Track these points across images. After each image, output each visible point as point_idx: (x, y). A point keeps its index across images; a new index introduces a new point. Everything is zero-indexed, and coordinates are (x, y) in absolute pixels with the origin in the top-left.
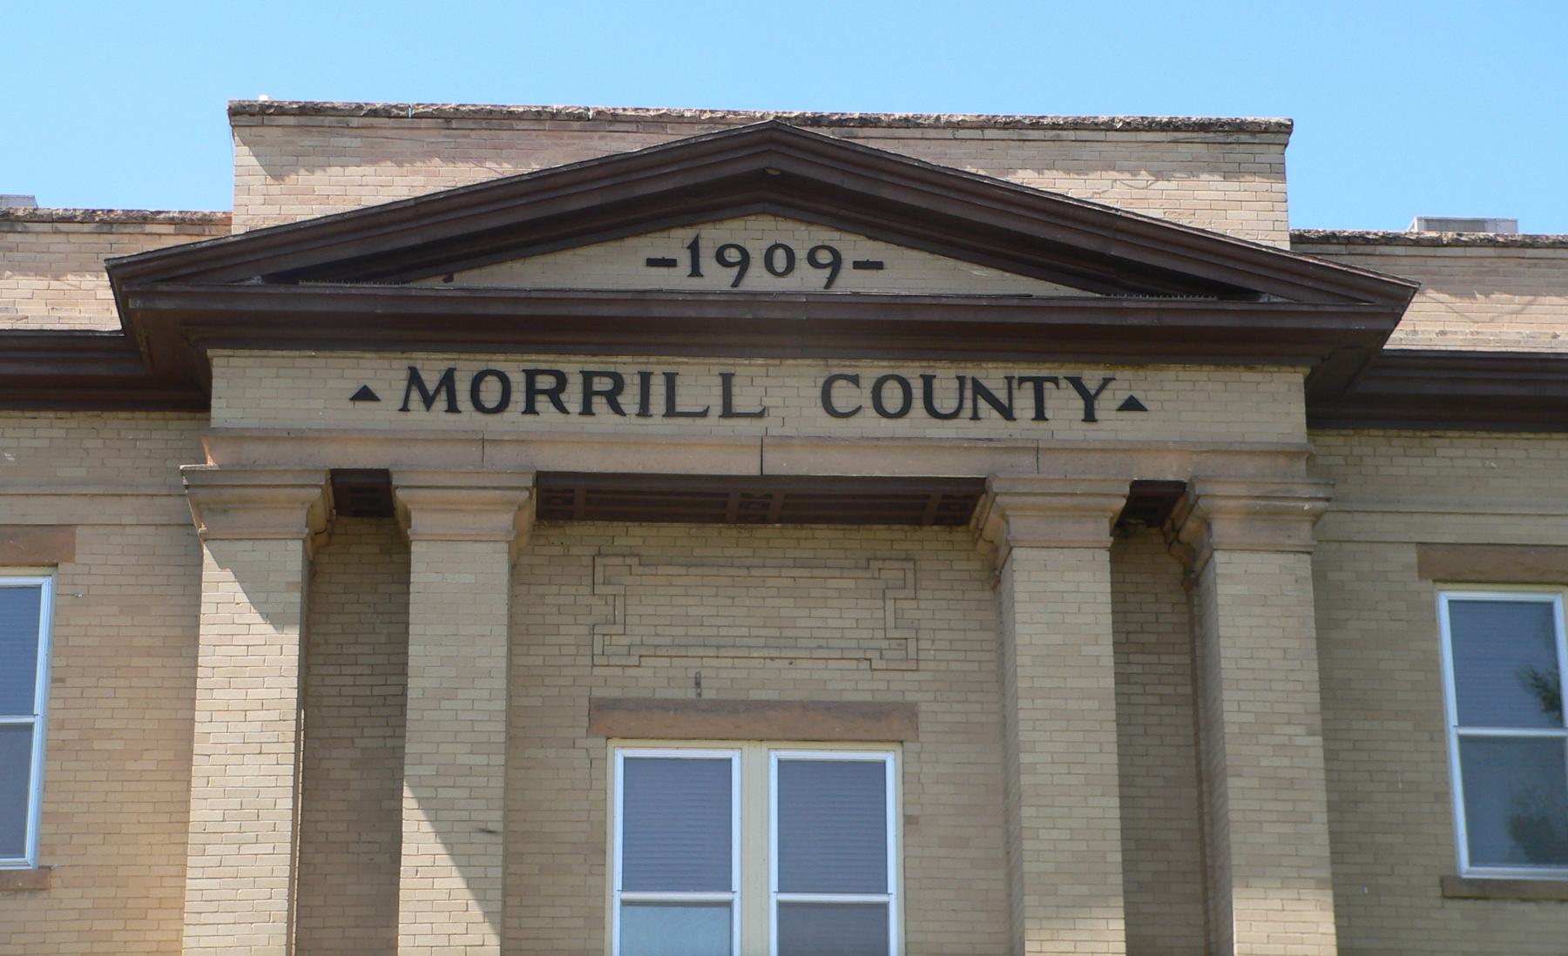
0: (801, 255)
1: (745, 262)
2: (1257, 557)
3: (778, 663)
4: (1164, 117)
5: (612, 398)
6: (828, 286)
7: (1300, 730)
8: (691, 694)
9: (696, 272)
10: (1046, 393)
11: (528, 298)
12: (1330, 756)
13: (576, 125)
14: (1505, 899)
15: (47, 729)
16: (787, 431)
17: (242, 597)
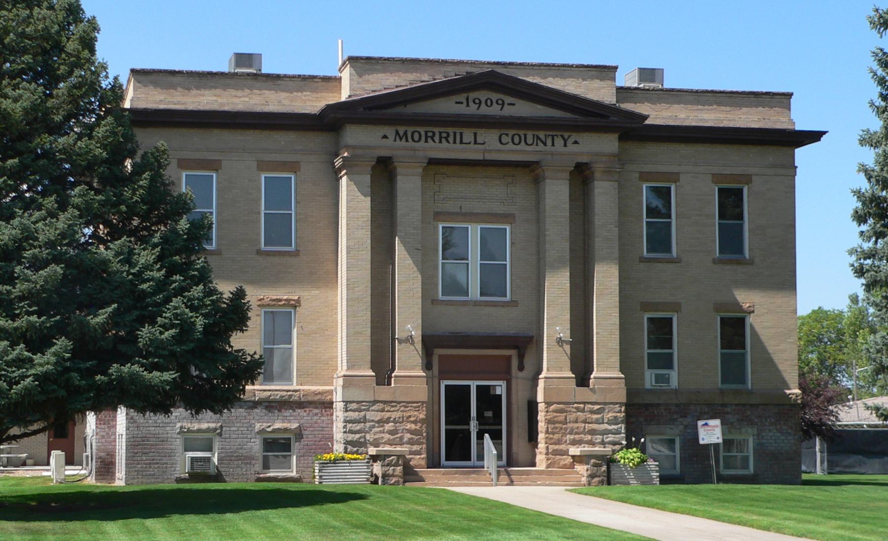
0: (494, 101)
7: (613, 226)
8: (459, 211)
9: (468, 105)
13: (436, 63)
17: (356, 189)
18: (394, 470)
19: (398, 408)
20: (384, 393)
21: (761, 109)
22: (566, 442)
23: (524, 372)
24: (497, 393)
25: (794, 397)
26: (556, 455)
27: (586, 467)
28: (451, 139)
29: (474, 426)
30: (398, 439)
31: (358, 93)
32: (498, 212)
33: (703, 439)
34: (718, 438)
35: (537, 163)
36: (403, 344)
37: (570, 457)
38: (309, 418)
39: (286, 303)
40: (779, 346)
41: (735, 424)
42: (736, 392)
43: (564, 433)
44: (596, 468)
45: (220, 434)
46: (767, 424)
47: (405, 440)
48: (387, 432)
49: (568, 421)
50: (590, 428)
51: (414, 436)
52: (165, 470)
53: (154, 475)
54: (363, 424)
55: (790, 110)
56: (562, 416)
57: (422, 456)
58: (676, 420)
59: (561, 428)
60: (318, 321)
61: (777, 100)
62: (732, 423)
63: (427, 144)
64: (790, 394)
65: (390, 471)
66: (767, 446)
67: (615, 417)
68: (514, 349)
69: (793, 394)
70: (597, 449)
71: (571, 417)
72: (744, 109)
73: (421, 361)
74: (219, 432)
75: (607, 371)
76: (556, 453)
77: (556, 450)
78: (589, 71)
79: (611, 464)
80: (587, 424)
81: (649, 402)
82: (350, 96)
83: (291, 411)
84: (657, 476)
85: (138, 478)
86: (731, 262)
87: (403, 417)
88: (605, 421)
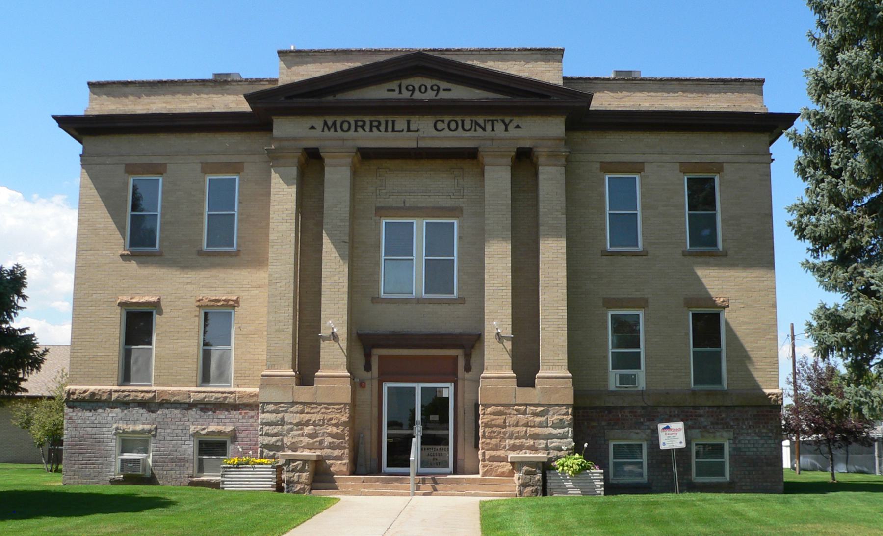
0: (429, 87)
1: (414, 90)
2: (551, 167)
3: (426, 197)
4: (529, 47)
6: (411, 96)
7: (560, 213)
8: (402, 205)
9: (400, 92)
10: (495, 124)
11: (353, 101)
12: (567, 219)
13: (369, 53)
14: (617, 256)
15: (238, 215)
16: (425, 136)
17: (282, 182)
18: (299, 476)
19: (318, 410)
20: (305, 393)
22: (505, 447)
23: (470, 373)
24: (444, 396)
25: (774, 397)
26: (493, 462)
28: (382, 128)
29: (418, 431)
30: (318, 443)
32: (444, 206)
34: (681, 443)
37: (509, 464)
38: (245, 421)
39: (225, 303)
40: (757, 343)
41: (708, 427)
42: (709, 393)
43: (503, 438)
44: (528, 477)
45: (155, 436)
46: (744, 427)
49: (507, 424)
50: (532, 433)
51: (335, 440)
54: (280, 427)
56: (501, 419)
57: (344, 462)
58: (642, 423)
60: (257, 322)
61: (747, 86)
62: (705, 427)
63: (357, 133)
64: (769, 394)
65: (295, 477)
66: (745, 451)
67: (561, 420)
68: (459, 348)
69: (773, 395)
70: (539, 455)
71: (511, 420)
73: (346, 360)
74: (153, 433)
75: (552, 370)
77: (494, 456)
78: (532, 54)
79: (547, 472)
80: (529, 428)
81: (612, 405)
83: (226, 413)
84: (601, 485)
85: (74, 478)
87: (324, 420)
88: (549, 425)
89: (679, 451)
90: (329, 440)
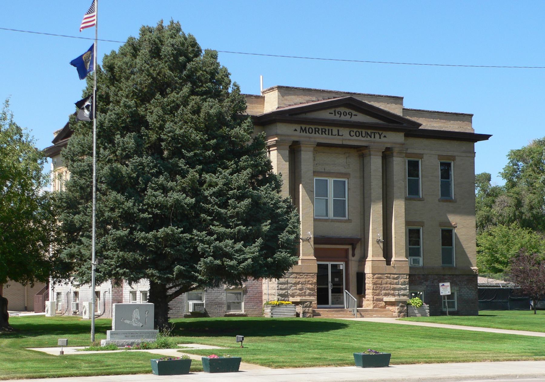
0: (347, 113)
5: (325, 132)
8: (324, 171)
9: (335, 115)
17: (281, 158)
21: (459, 122)
25: (475, 271)
27: (397, 308)
28: (327, 133)
31: (282, 106)
33: (442, 293)
35: (366, 147)
36: (305, 242)
43: (381, 290)
47: (307, 293)
48: (298, 289)
52: (179, 310)
53: (173, 313)
55: (471, 123)
59: (380, 287)
67: (405, 281)
71: (384, 281)
72: (452, 122)
76: (378, 300)
82: (278, 108)
86: (446, 201)
89: (448, 296)
90: (308, 291)
